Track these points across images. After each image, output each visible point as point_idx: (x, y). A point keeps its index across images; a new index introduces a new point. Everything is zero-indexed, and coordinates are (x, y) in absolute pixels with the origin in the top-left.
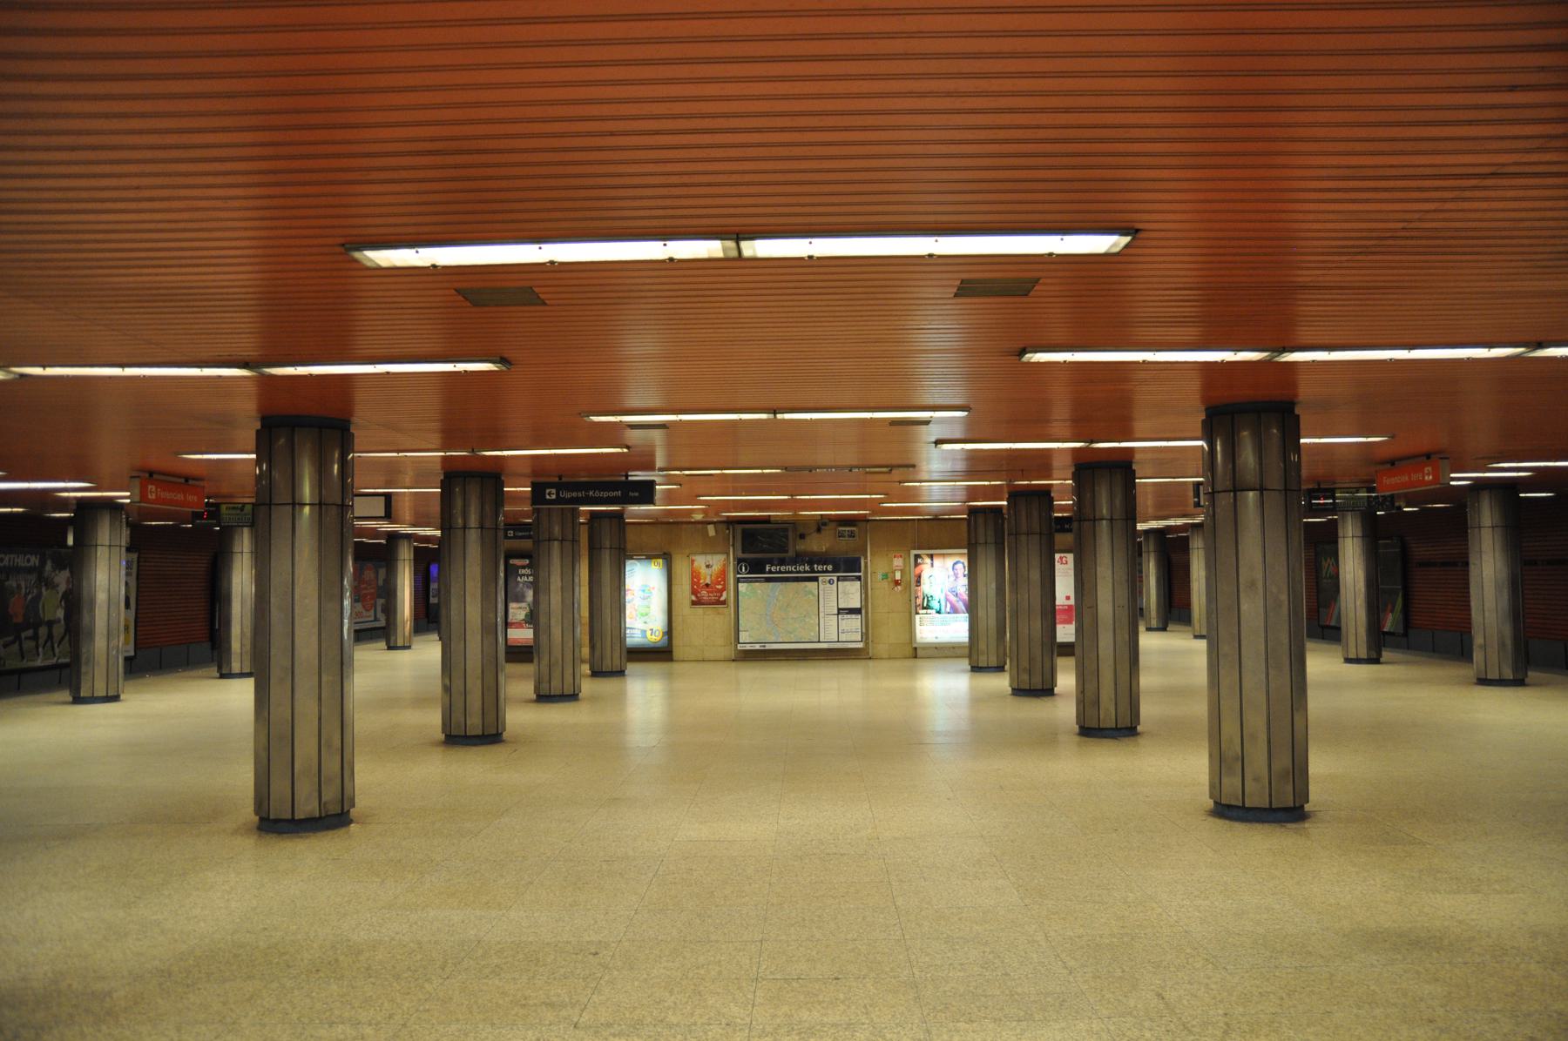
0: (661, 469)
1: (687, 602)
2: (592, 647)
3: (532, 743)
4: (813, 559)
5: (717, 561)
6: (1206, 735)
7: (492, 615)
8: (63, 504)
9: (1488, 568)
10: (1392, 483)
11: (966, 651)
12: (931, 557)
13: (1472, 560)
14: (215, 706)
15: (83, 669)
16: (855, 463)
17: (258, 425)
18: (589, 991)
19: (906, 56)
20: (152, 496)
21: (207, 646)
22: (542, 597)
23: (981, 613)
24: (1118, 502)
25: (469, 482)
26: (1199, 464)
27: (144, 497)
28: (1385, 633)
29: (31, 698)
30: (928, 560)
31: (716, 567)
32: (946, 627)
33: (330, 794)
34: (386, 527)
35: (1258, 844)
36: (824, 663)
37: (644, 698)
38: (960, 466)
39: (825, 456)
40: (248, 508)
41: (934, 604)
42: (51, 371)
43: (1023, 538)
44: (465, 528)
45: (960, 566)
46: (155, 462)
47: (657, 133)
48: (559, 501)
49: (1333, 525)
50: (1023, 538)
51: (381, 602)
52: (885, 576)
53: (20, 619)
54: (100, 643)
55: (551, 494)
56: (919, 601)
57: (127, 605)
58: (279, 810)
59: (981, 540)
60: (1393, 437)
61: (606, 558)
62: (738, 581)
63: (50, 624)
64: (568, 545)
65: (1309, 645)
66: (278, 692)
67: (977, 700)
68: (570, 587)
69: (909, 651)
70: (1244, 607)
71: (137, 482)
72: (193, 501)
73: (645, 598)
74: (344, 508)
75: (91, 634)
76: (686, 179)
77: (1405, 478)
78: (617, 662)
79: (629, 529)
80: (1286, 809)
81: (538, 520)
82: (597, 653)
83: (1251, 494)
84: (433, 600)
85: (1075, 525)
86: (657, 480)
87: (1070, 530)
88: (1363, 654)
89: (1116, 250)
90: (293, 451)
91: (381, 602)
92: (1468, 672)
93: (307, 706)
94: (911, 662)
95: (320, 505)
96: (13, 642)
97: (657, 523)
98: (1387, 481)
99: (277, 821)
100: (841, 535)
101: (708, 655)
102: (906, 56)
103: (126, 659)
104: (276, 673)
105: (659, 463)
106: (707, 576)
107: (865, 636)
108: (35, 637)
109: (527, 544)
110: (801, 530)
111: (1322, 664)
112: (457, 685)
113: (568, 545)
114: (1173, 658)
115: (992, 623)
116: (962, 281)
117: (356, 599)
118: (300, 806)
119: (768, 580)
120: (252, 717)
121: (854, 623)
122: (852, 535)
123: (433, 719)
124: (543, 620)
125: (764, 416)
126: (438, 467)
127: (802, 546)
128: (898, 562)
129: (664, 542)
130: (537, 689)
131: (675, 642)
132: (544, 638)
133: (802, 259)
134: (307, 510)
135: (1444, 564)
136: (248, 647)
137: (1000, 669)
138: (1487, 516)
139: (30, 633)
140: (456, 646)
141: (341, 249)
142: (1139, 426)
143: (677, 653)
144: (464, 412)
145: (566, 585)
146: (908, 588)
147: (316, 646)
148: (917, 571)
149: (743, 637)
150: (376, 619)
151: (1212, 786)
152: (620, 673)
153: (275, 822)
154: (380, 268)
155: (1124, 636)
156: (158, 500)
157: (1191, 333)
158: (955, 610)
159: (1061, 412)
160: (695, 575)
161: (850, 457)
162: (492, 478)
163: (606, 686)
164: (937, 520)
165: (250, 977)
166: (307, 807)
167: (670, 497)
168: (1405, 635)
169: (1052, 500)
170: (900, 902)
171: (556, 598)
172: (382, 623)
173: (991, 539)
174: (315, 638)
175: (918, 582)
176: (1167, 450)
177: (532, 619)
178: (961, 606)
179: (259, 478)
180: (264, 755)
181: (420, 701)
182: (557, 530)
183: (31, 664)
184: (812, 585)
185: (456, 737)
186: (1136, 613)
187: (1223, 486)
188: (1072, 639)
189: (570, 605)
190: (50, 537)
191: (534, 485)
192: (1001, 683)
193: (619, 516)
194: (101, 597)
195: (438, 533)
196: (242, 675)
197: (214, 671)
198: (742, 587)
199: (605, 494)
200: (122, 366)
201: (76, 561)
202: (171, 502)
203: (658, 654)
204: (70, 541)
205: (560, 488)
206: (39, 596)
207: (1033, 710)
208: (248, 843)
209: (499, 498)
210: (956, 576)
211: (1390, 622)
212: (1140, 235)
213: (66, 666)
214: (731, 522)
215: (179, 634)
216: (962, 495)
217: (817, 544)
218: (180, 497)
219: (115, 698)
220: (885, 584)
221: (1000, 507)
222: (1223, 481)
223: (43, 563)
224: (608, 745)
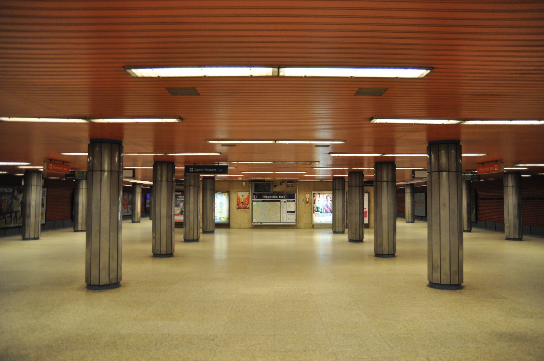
1: (236, 208)
2: (203, 223)
3: (184, 257)
4: (278, 194)
5: (246, 194)
6: (427, 258)
7: (170, 212)
8: (21, 171)
9: (511, 200)
11: (331, 226)
12: (319, 194)
13: (505, 198)
15: (26, 228)
17: (89, 142)
18: (212, 356)
20: (51, 168)
21: (71, 220)
22: (187, 206)
23: (337, 213)
24: (390, 176)
25: (163, 165)
27: (48, 168)
30: (318, 195)
33: (113, 276)
35: (446, 297)
36: (282, 230)
37: (220, 240)
40: (85, 173)
41: (320, 210)
43: (353, 188)
44: (161, 181)
45: (329, 197)
46: (53, 155)
47: (258, 16)
48: (194, 172)
50: (353, 188)
51: (129, 206)
52: (303, 200)
53: (5, 210)
54: (32, 219)
55: (191, 170)
57: (43, 206)
58: (94, 281)
59: (337, 188)
60: (488, 154)
61: (208, 192)
63: (16, 212)
64: (196, 188)
67: (335, 243)
68: (196, 202)
69: (311, 226)
70: (442, 213)
71: (46, 163)
73: (221, 206)
74: (119, 172)
75: (29, 216)
77: (487, 169)
79: (216, 183)
80: (455, 285)
81: (185, 179)
82: (205, 225)
84: (148, 206)
87: (373, 186)
90: (101, 152)
91: (129, 206)
92: (504, 235)
93: (105, 244)
94: (312, 230)
95: (111, 171)
96: (2, 218)
97: (226, 181)
99: (94, 285)
101: (242, 226)
103: (42, 225)
104: (94, 232)
106: (242, 199)
107: (296, 220)
108: (11, 217)
112: (158, 236)
113: (196, 188)
114: (411, 232)
115: (341, 216)
116: (360, 89)
117: (123, 205)
118: (102, 280)
119: (263, 201)
120: (151, 231)
121: (292, 216)
122: (292, 186)
123: (149, 248)
124: (187, 214)
125: (271, 142)
126: (152, 160)
128: (308, 195)
129: (228, 188)
130: (185, 237)
131: (231, 221)
132: (187, 220)
134: (106, 174)
135: (489, 199)
136: (84, 221)
137: (343, 232)
138: (510, 183)
139: (9, 215)
140: (157, 222)
141: (122, 69)
142: (397, 149)
143: (232, 225)
144: (162, 138)
145: (194, 201)
147: (108, 222)
149: (254, 220)
150: (128, 212)
151: (429, 276)
152: (213, 232)
153: (93, 286)
154: (137, 78)
155: (391, 222)
156: (53, 170)
158: (327, 212)
160: (238, 199)
162: (171, 163)
163: (207, 237)
164: (322, 181)
165: (83, 349)
166: (104, 280)
168: (476, 222)
169: (363, 175)
170: (323, 319)
171: (192, 206)
172: (130, 213)
173: (340, 188)
174: (108, 219)
175: (314, 203)
176: (411, 159)
178: (329, 211)
179: (89, 163)
181: (143, 241)
182: (192, 182)
183: (9, 226)
184: (278, 203)
185: (157, 255)
187: (434, 169)
189: (196, 208)
190: (16, 182)
191: (186, 167)
192: (345, 237)
193: (213, 178)
194: (33, 203)
195: (151, 183)
196: (82, 231)
197: (72, 229)
198: (254, 203)
199: (211, 170)
200: (39, 117)
201: (25, 190)
202: (58, 170)
204: (23, 184)
205: (194, 167)
206: (12, 202)
208: (83, 295)
209: (174, 171)
210: (327, 201)
211: (473, 219)
213: (19, 227)
215: (62, 215)
217: (278, 189)
218: (61, 168)
219: (37, 238)
220: (303, 203)
221: (344, 177)
223: (14, 191)
224: (208, 258)
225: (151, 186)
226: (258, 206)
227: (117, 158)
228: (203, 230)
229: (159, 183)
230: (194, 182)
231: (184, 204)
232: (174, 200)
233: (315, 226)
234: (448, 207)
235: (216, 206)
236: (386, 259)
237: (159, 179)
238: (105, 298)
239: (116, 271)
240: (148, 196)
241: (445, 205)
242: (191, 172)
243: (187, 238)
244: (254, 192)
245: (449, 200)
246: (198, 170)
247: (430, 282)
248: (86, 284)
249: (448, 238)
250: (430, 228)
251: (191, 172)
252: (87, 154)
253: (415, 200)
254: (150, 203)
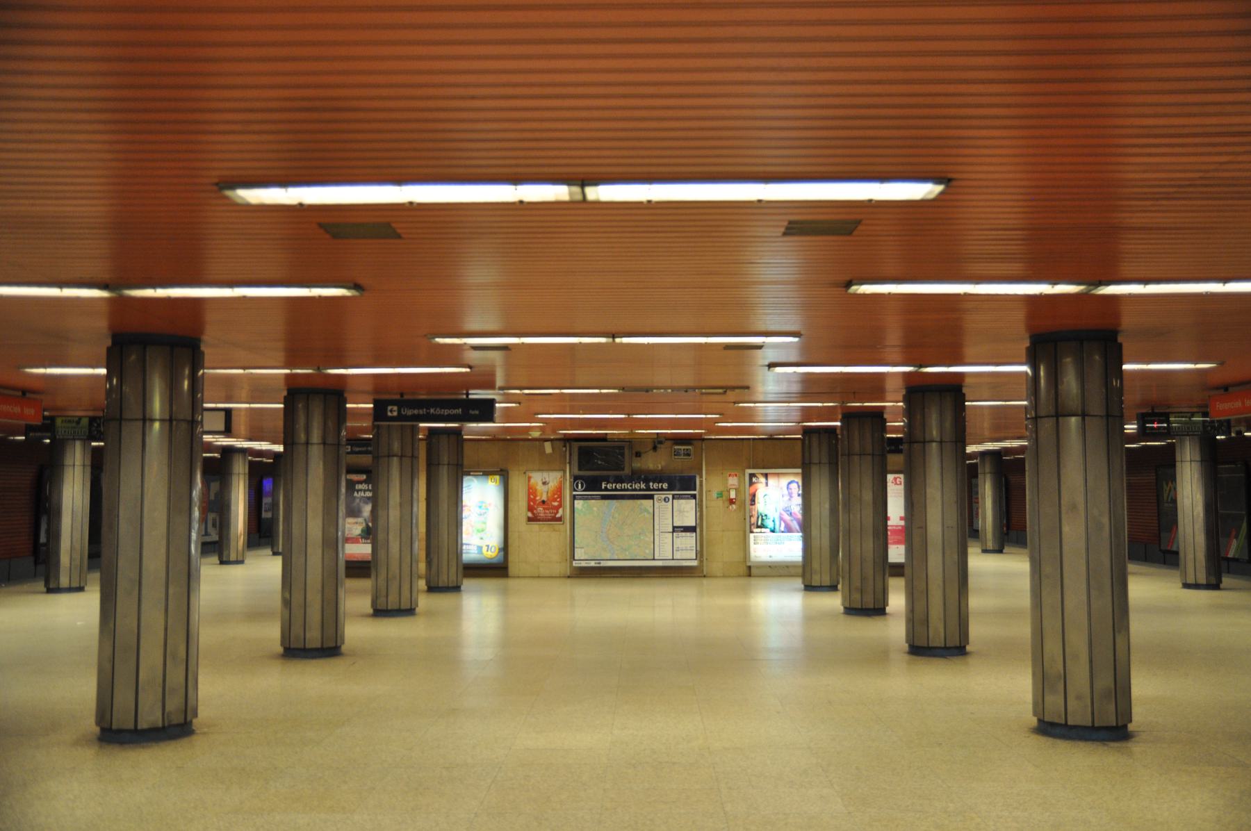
0: (501, 388)
1: (524, 519)
3: (371, 655)
5: (553, 478)
10: (1225, 408)
11: (800, 571)
12: (766, 476)
16: (691, 384)
17: (109, 342)
19: (734, 40)
21: (32, 559)
22: (381, 513)
23: (815, 532)
24: (948, 424)
25: (311, 399)
26: (1023, 388)
28: (1228, 560)
29: (18, 588)
30: (763, 480)
31: (553, 484)
32: (779, 546)
33: (174, 704)
37: (479, 613)
38: (796, 388)
39: (662, 377)
40: (85, 422)
41: (769, 524)
43: (856, 458)
44: (307, 443)
45: (794, 486)
48: (400, 418)
49: (1172, 447)
50: (856, 458)
52: (720, 495)
55: (393, 411)
56: (753, 520)
58: (122, 719)
59: (815, 459)
60: (1222, 364)
61: (444, 474)
62: (574, 498)
64: (407, 461)
65: (1131, 567)
66: (124, 604)
67: (810, 618)
69: (743, 570)
70: (1066, 529)
72: (31, 414)
74: (193, 423)
76: (537, 135)
77: (1238, 404)
78: (453, 577)
79: (466, 446)
80: (1110, 728)
81: (377, 436)
83: (1073, 419)
84: (266, 515)
85: (904, 447)
86: (497, 398)
87: (900, 451)
88: (1202, 579)
89: (932, 196)
93: (153, 618)
95: (170, 421)
97: (495, 439)
98: (1221, 406)
99: (120, 731)
100: (677, 453)
101: (543, 571)
102: (734, 40)
104: (123, 585)
105: (499, 382)
106: (543, 493)
107: (700, 554)
109: (366, 460)
112: (297, 599)
113: (407, 461)
115: (826, 542)
116: (790, 222)
118: (142, 718)
120: (280, 586)
121: (689, 540)
123: (272, 633)
127: (637, 464)
128: (733, 481)
129: (501, 460)
131: (511, 558)
132: (382, 554)
133: (641, 203)
134: (157, 425)
137: (833, 588)
140: (297, 560)
141: (215, 188)
142: (969, 351)
143: (512, 569)
144: (307, 332)
145: (405, 499)
146: (742, 506)
148: (752, 489)
149: (579, 554)
151: (1035, 704)
152: (456, 589)
157: (1016, 268)
158: (789, 529)
159: (894, 337)
161: (686, 379)
162: (334, 395)
163: (442, 601)
164: (772, 439)
166: (150, 716)
167: (508, 415)
169: (885, 421)
171: (394, 514)
173: (825, 460)
175: (753, 501)
176: (995, 375)
177: (369, 533)
178: (795, 525)
179: (109, 393)
180: (108, 666)
182: (396, 446)
184: (647, 503)
185: (295, 650)
186: (969, 531)
187: (1047, 411)
188: (901, 559)
191: (376, 402)
193: (457, 433)
195: (279, 448)
197: (41, 586)
198: (579, 504)
199: (446, 412)
203: (494, 570)
205: (400, 404)
207: (867, 629)
208: (88, 754)
210: (790, 495)
211: (1234, 548)
212: (954, 183)
214: (568, 440)
216: (796, 416)
217: (652, 462)
218: (17, 410)
220: (720, 503)
221: (834, 428)
222: (1046, 407)
224: (444, 657)
225: (277, 456)
226: (591, 514)
227: (186, 383)
228: (428, 583)
229: (301, 449)
231: (374, 511)
232: (343, 497)
233: (754, 571)
234: (1082, 513)
235: (465, 514)
237: (303, 437)
238: (151, 763)
239: (183, 690)
240: (268, 485)
241: (1074, 507)
242: (393, 419)
243: (381, 606)
244: (576, 472)
245: (1079, 494)
246: (410, 412)
247: (1039, 720)
248: (97, 729)
249: (1085, 598)
251: (393, 419)
252: (103, 371)
254: (274, 506)
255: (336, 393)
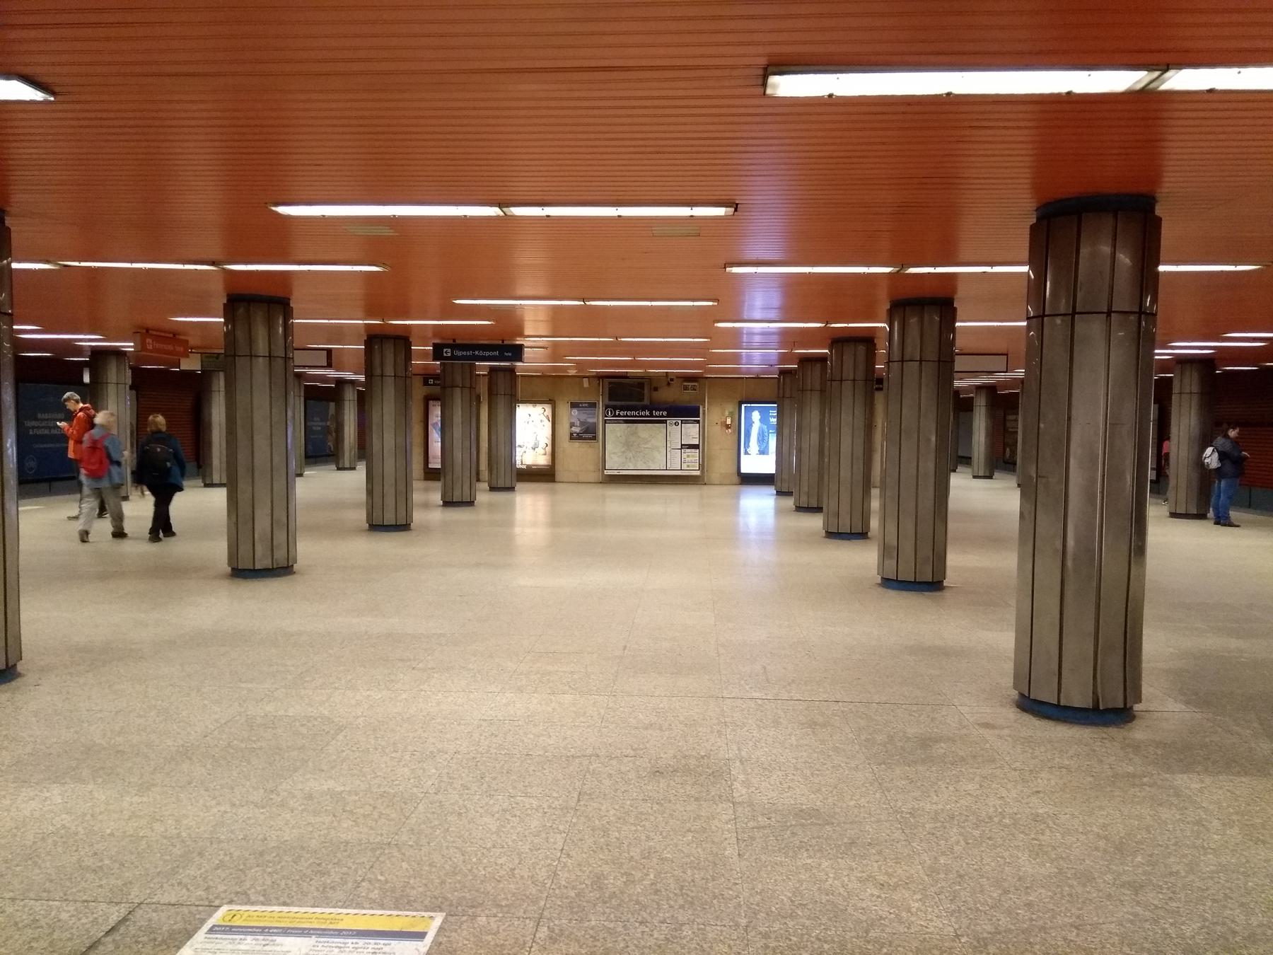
8: (79, 351)
14: (352, 482)
27: (144, 347)
32: (760, 461)
34: (331, 373)
37: (529, 506)
42: (83, 264)
46: (151, 321)
58: (245, 564)
62: (605, 422)
73: (532, 431)
82: (494, 476)
88: (981, 474)
100: (686, 388)
101: (581, 479)
107: (702, 467)
110: (655, 385)
111: (1156, 512)
113: (466, 391)
123: (361, 516)
126: (362, 331)
131: (557, 467)
133: (1059, 95)
143: (560, 475)
152: (511, 489)
153: (242, 572)
179: (226, 335)
191: (435, 345)
192: (864, 559)
193: (512, 370)
196: (220, 485)
199: (487, 354)
203: (542, 476)
204: (87, 379)
205: (457, 351)
214: (601, 377)
218: (170, 347)
220: (718, 428)
221: (867, 340)
222: (896, 355)
226: (615, 433)
230: (463, 379)
236: (846, 543)
246: (460, 353)
250: (1028, 491)
253: (1007, 427)
255: (402, 340)
